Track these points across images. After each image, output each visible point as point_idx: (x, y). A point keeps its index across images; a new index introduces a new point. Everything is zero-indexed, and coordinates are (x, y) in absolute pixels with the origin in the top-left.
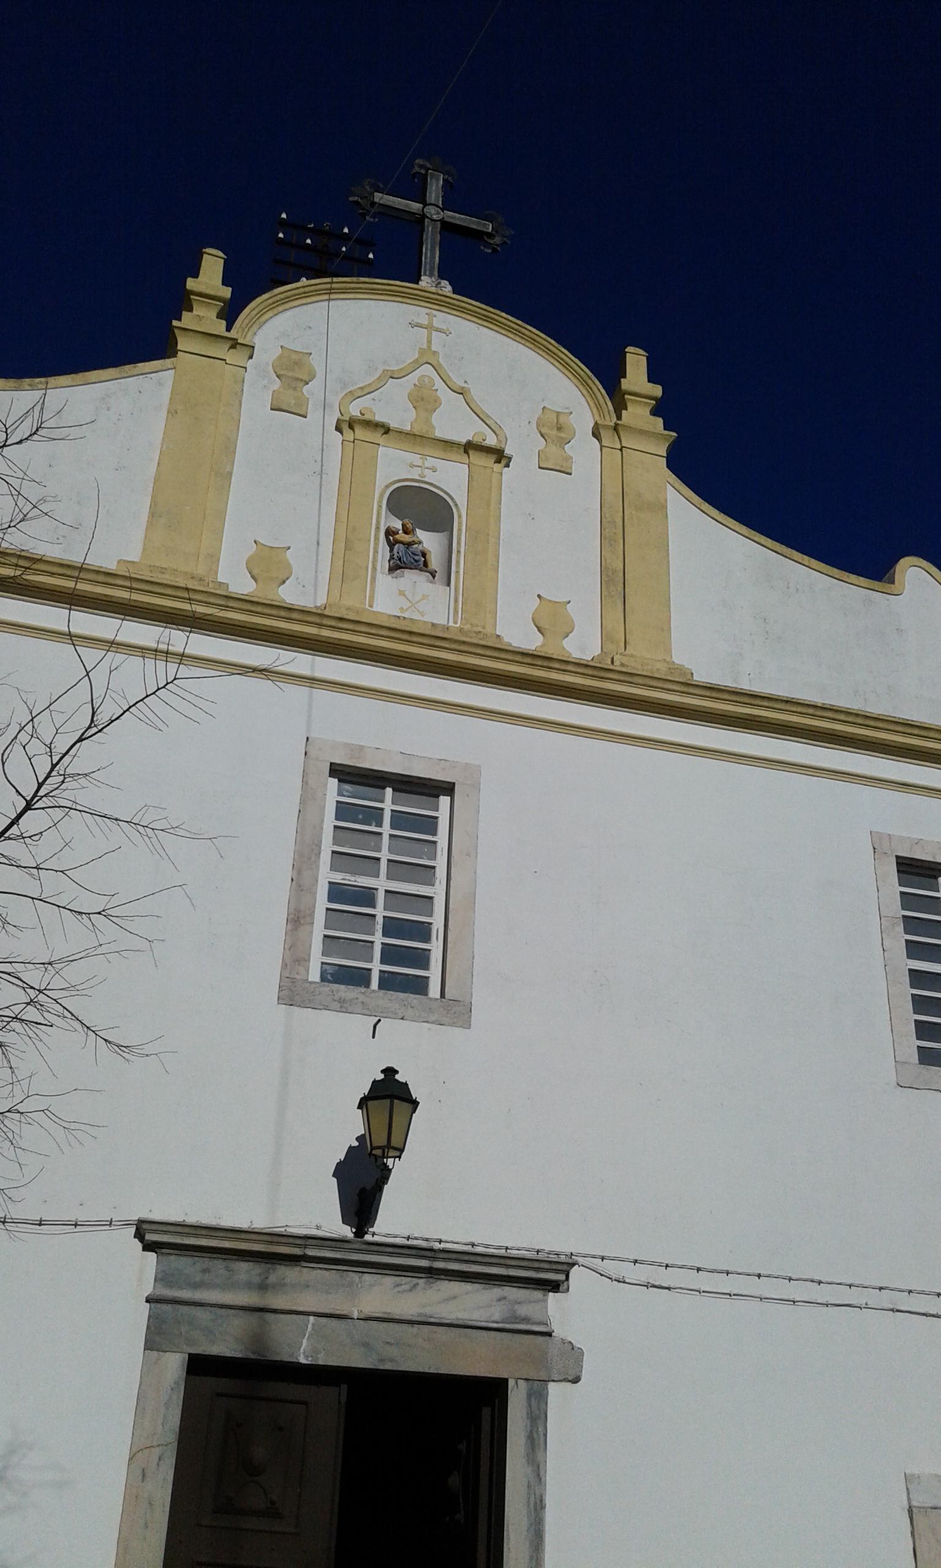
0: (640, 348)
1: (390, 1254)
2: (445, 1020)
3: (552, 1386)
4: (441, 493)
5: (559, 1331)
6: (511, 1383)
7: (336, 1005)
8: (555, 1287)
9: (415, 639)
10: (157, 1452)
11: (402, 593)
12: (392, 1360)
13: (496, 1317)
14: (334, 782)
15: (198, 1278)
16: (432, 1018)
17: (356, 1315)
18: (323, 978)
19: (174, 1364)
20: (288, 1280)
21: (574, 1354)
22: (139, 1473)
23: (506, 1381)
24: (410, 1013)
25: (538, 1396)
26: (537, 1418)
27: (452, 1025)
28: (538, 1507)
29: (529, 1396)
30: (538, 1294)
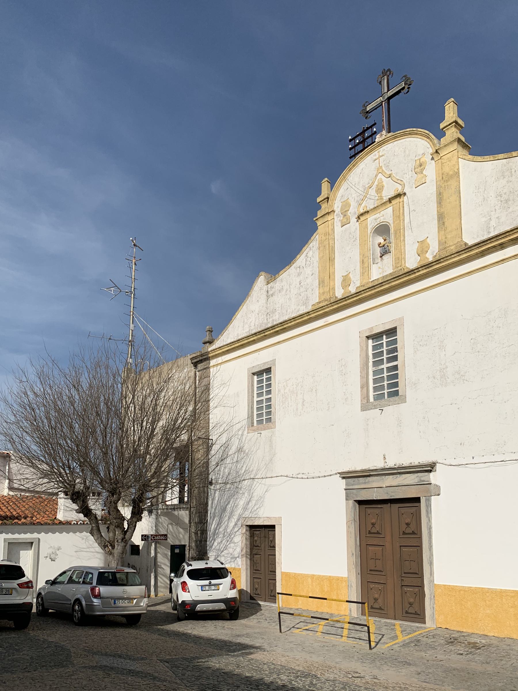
0: (286, 266)
1: (388, 471)
2: (400, 402)
3: (432, 497)
4: (384, 223)
5: (433, 482)
6: (421, 498)
7: (373, 407)
8: (430, 471)
9: (376, 287)
10: (350, 522)
11: (379, 268)
12: (394, 496)
13: (416, 482)
14: (370, 341)
15: (353, 483)
16: (397, 403)
17: (384, 486)
18: (375, 400)
19: (351, 502)
20: (370, 481)
21: (438, 487)
22: (348, 527)
23: (420, 497)
24: (391, 403)
25: (428, 501)
26: (429, 506)
27: (402, 403)
28: (430, 528)
29: (426, 500)
30: (427, 474)
